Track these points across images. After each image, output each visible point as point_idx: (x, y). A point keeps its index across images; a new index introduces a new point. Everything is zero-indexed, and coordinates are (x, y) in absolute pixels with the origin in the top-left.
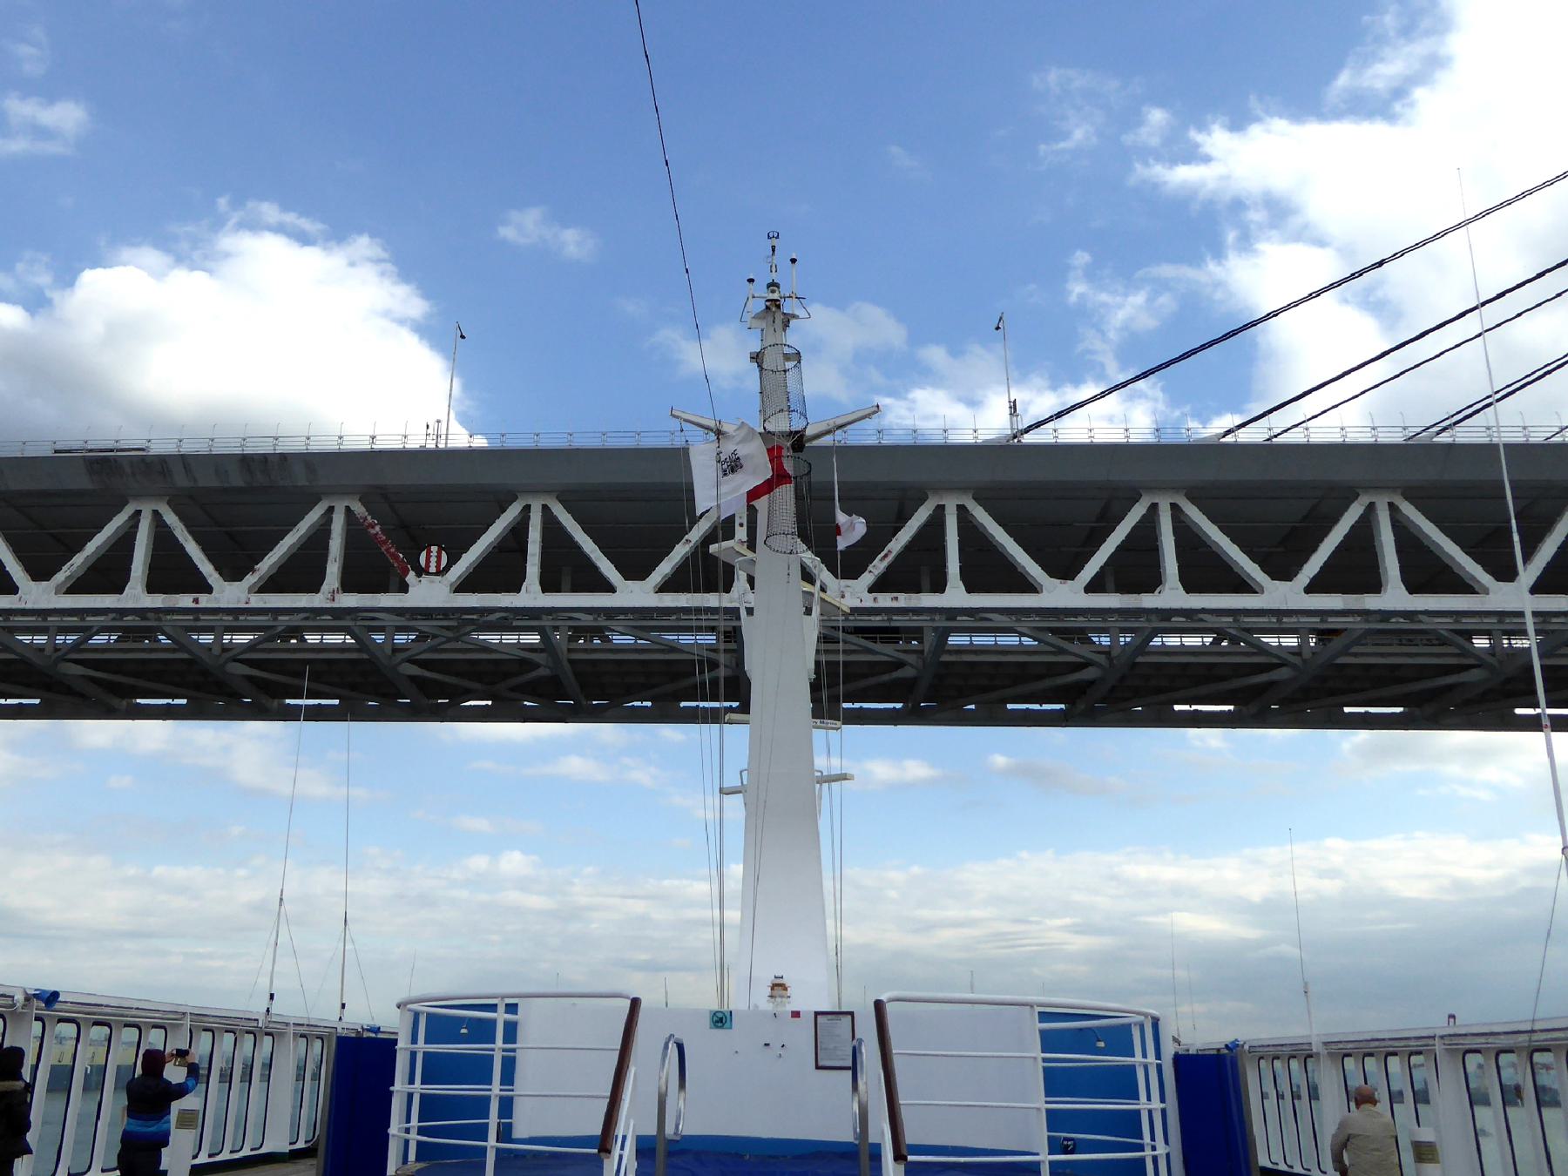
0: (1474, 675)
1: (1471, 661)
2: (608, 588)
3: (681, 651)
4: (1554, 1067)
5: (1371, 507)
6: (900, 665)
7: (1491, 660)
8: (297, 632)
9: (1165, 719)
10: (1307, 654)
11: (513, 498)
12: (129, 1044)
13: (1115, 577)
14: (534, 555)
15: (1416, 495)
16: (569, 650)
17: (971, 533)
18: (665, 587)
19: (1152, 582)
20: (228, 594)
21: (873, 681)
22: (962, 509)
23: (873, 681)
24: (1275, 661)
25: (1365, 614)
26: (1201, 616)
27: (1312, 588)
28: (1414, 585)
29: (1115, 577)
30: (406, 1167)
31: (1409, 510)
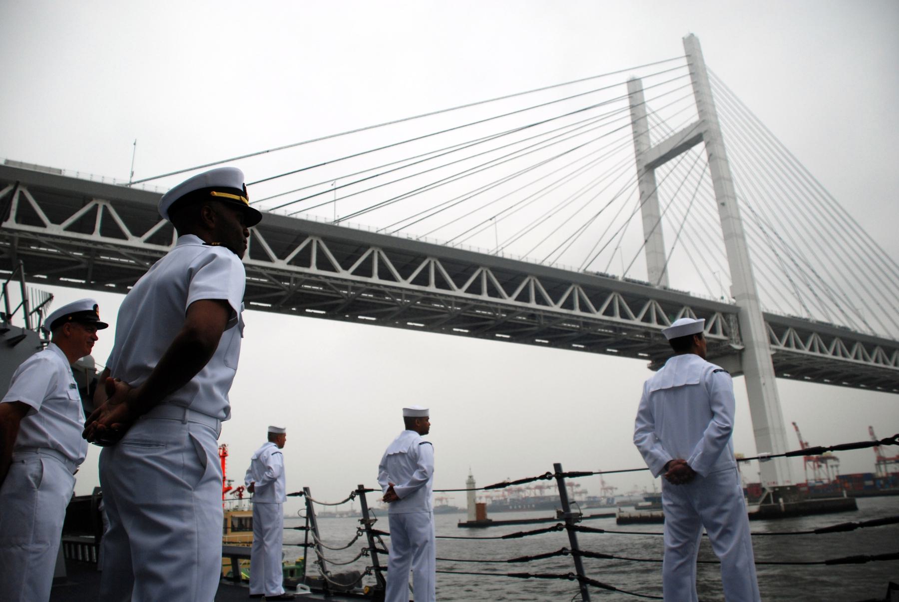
0: (574, 334)
1: (340, 296)
2: (43, 225)
3: (73, 257)
4: (394, 484)
5: (312, 241)
6: (533, 326)
7: (346, 297)
8: (561, 322)
9: (301, 313)
10: (349, 296)
11: (91, 200)
12: (230, 503)
13: (524, 297)
14: (14, 210)
15: (325, 239)
16: (19, 249)
17: (107, 216)
18: (69, 229)
19: (91, 231)
20: (281, 264)
21: (70, 268)
22: (105, 208)
23: (70, 268)
24: (281, 288)
25: (366, 283)
26: (254, 267)
27: (354, 273)
28: (381, 277)
29: (295, 262)
30: (664, 598)
31: (438, 263)
